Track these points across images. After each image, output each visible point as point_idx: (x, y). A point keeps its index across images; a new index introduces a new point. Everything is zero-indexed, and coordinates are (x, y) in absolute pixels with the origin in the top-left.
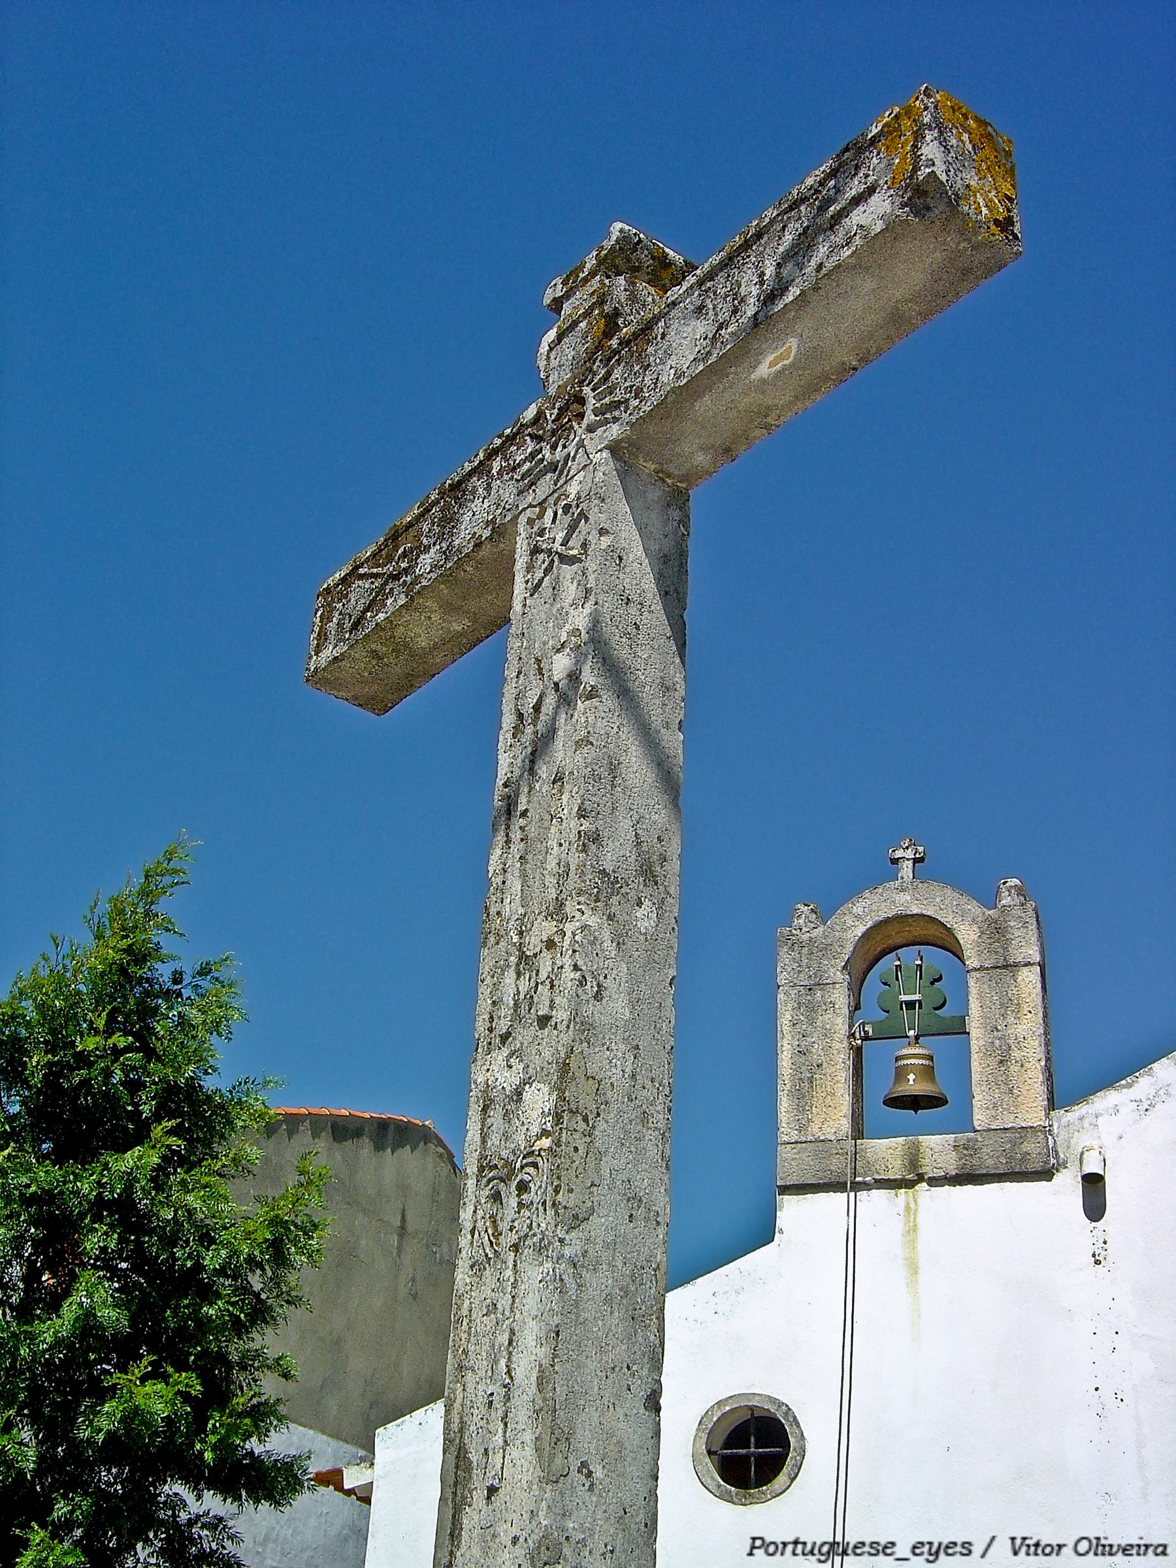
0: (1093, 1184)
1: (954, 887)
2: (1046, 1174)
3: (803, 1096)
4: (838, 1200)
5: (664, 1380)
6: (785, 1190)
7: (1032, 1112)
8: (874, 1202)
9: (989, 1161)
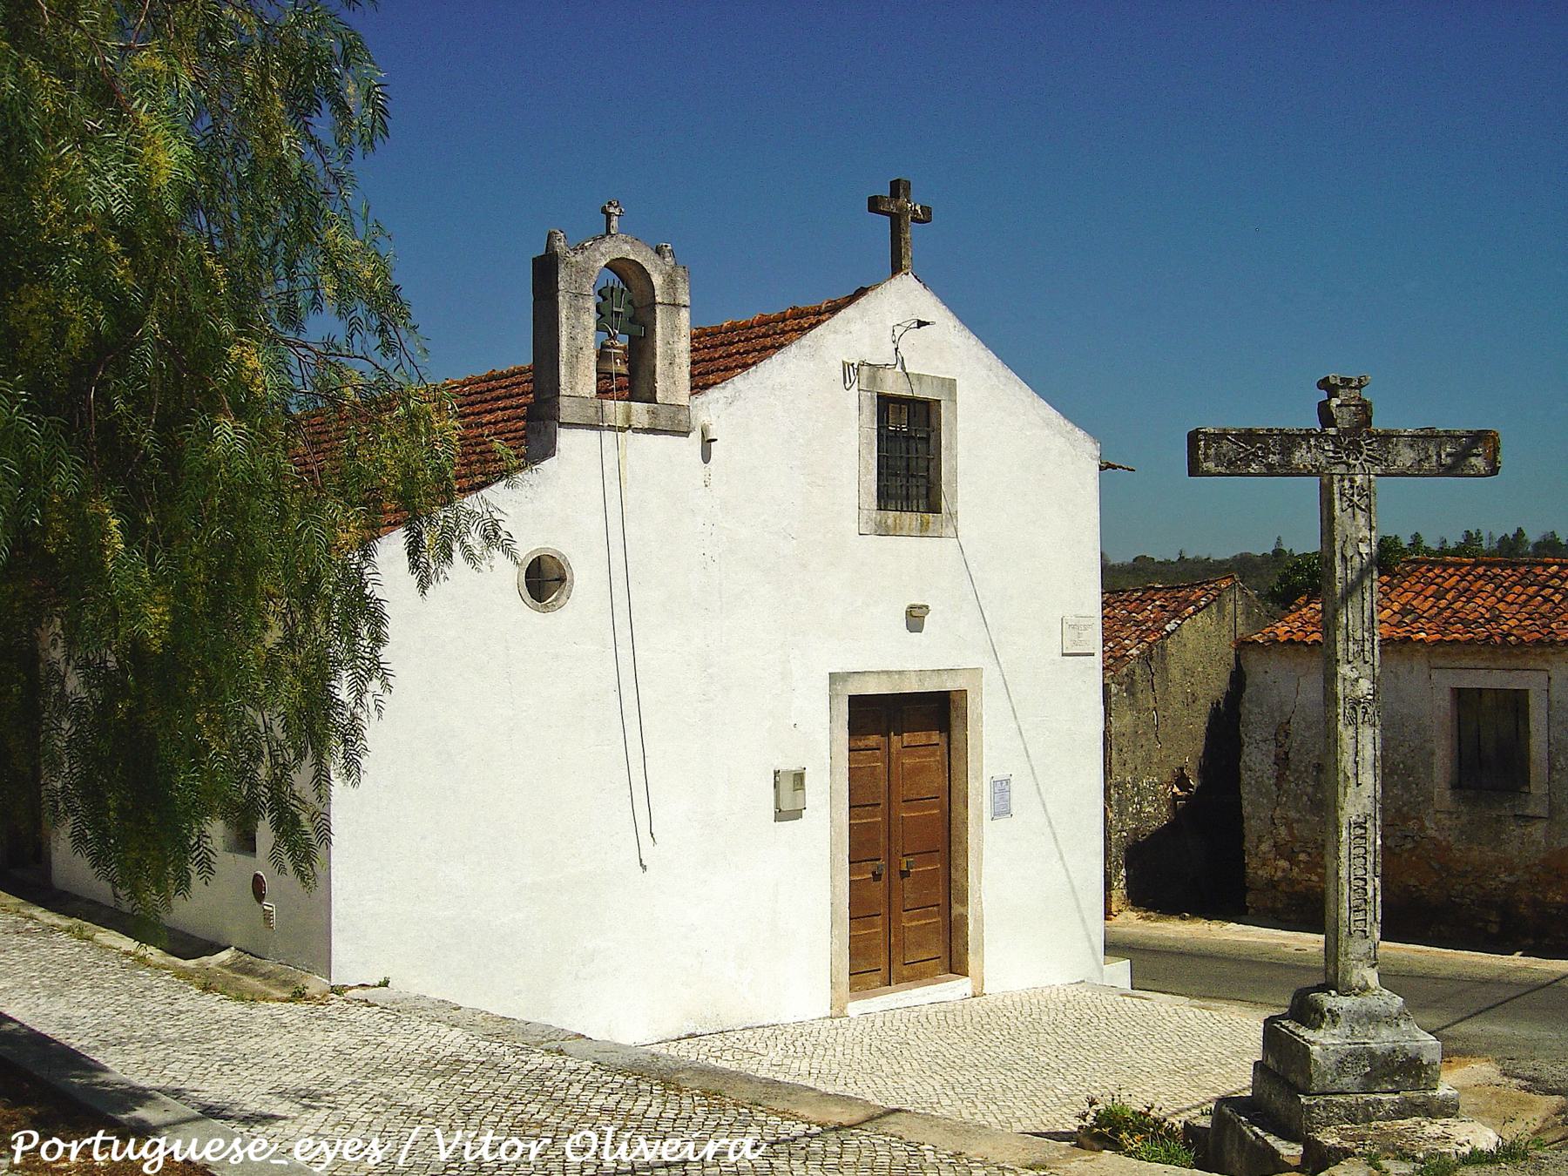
0: (707, 443)
1: (1237, 756)
2: (686, 434)
3: (572, 368)
4: (595, 434)
5: (1223, 551)
6: (562, 425)
7: (684, 401)
8: (609, 436)
9: (662, 423)
